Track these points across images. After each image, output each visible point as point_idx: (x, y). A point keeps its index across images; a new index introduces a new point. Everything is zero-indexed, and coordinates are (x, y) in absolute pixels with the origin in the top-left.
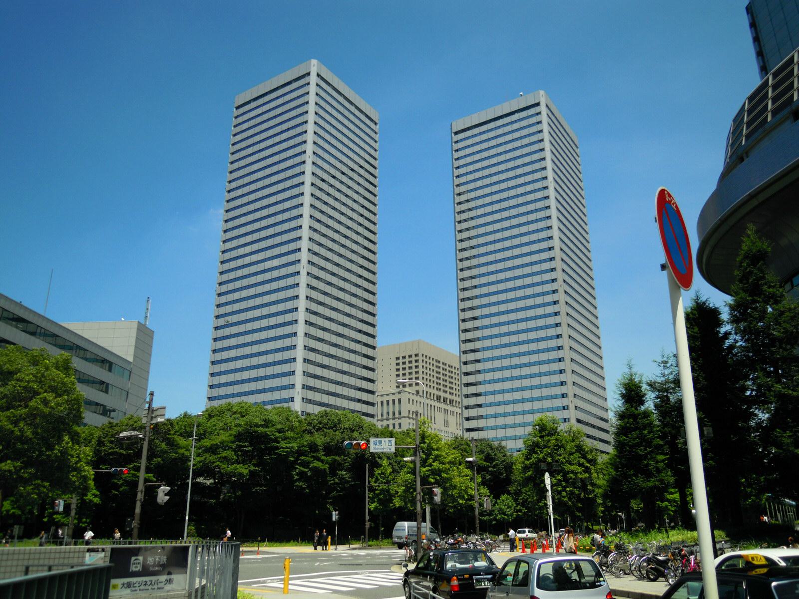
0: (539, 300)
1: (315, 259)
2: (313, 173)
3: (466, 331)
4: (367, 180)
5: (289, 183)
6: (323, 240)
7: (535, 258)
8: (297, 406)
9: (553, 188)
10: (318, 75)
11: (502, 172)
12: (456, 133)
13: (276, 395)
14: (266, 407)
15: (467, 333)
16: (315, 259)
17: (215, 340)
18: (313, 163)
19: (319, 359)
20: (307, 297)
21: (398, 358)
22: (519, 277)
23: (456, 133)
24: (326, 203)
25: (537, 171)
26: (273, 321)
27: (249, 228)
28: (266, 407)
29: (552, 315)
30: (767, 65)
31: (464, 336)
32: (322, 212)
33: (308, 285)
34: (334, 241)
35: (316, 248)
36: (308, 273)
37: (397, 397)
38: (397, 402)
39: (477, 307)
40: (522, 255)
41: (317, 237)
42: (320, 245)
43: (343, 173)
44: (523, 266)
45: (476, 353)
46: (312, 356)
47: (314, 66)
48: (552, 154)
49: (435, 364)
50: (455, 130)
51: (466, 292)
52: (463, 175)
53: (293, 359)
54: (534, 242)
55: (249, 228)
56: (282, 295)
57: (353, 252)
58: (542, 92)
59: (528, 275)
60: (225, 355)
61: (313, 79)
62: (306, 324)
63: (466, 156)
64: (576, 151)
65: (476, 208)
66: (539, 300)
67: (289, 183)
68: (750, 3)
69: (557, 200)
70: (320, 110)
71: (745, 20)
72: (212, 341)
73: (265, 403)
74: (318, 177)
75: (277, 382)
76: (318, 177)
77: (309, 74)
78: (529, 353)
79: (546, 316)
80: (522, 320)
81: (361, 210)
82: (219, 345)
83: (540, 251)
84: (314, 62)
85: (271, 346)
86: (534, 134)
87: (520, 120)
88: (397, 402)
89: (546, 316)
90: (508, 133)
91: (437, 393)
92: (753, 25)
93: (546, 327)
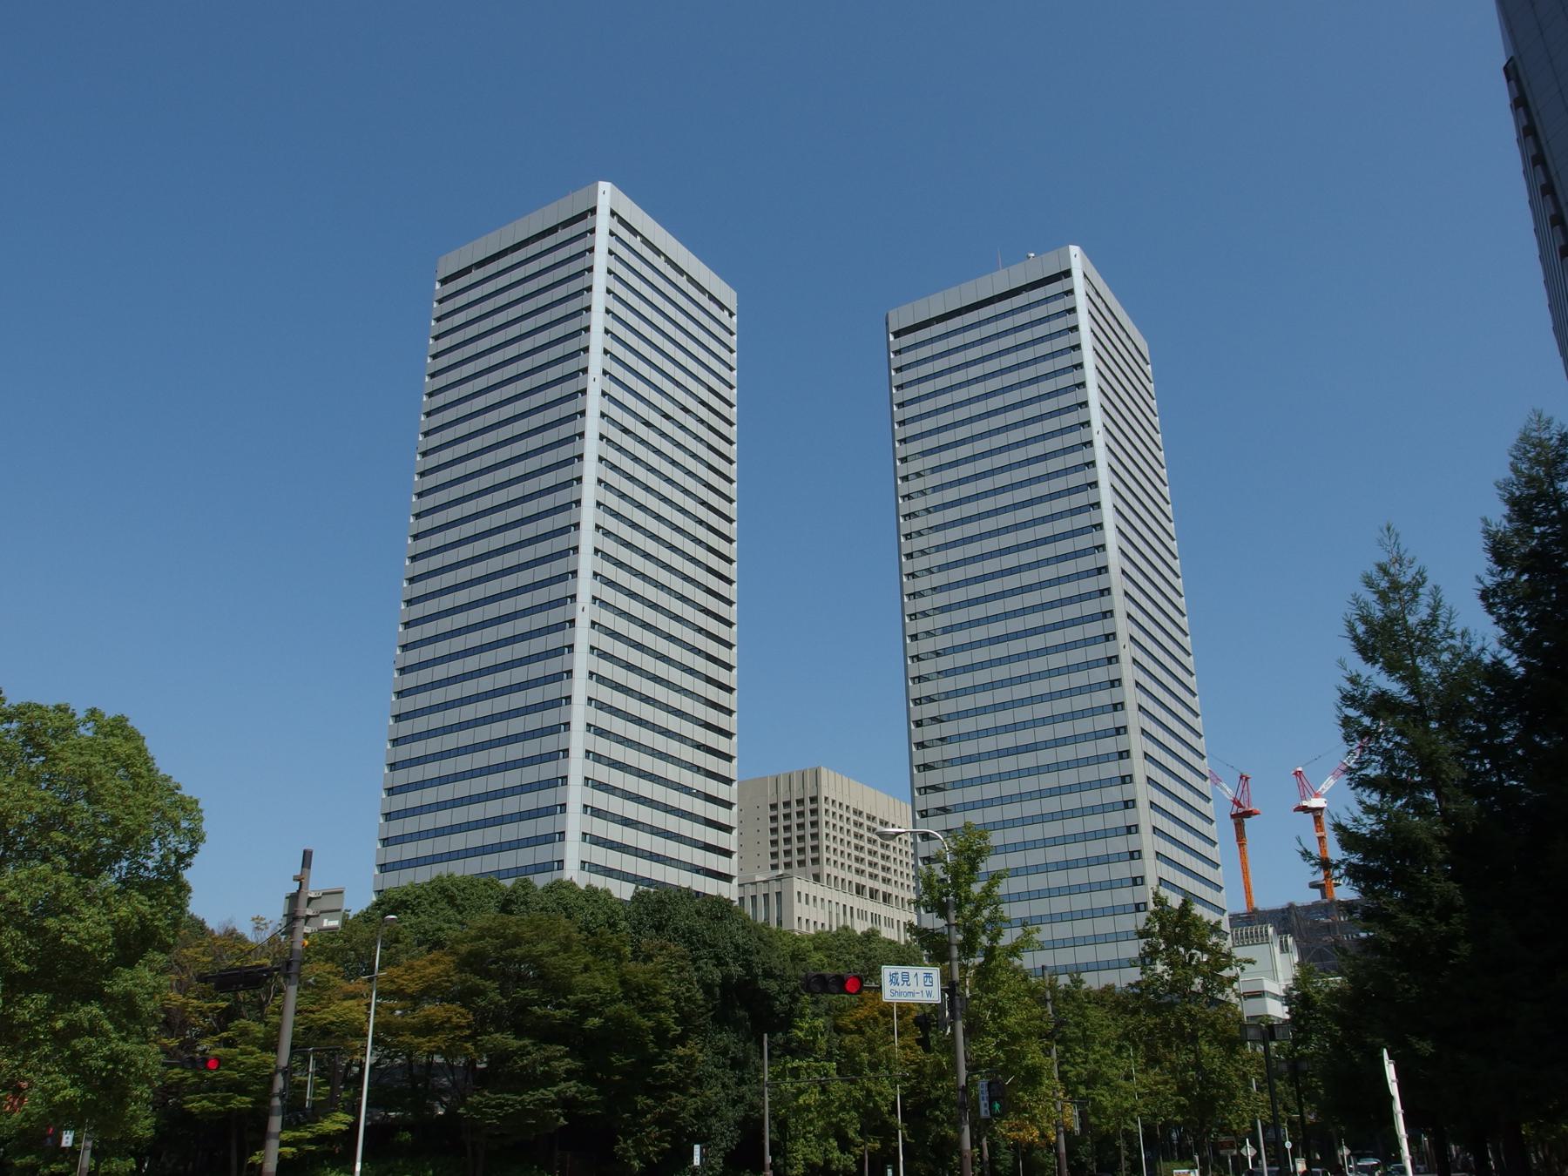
0: (1079, 679)
1: (609, 594)
2: (603, 415)
3: (926, 767)
4: (709, 680)
5: (557, 352)
6: (624, 555)
7: (1072, 611)
8: (572, 872)
9: (1109, 486)
10: (613, 213)
11: (996, 412)
12: (897, 334)
13: (526, 857)
14: (502, 882)
15: (928, 773)
16: (609, 594)
17: (391, 791)
18: (604, 394)
19: (616, 805)
20: (591, 674)
21: (774, 807)
22: (1044, 721)
23: (897, 334)
24: (631, 478)
25: (1064, 371)
26: (516, 726)
27: (468, 530)
28: (502, 882)
29: (1108, 733)
30: (1555, 180)
31: (923, 779)
32: (623, 496)
33: (592, 648)
34: (646, 556)
35: (607, 644)
36: (593, 623)
37: (775, 887)
38: (773, 899)
39: (950, 717)
40: (1052, 696)
41: (610, 547)
42: (616, 515)
43: (667, 416)
44: (1049, 673)
45: (942, 724)
46: (601, 800)
47: (606, 195)
48: (1102, 395)
49: (853, 817)
50: (894, 327)
51: (920, 601)
52: (913, 419)
53: (562, 778)
54: (1052, 414)
55: (468, 530)
56: (539, 620)
57: (686, 578)
58: (1074, 250)
59: (1061, 694)
60: (413, 799)
61: (603, 222)
62: (584, 840)
63: (921, 417)
64: (1148, 387)
65: (960, 737)
66: (1079, 679)
67: (557, 352)
68: (1511, 60)
69: (1123, 553)
70: (619, 245)
71: (1501, 95)
72: (386, 771)
73: (500, 874)
74: (613, 422)
75: (539, 620)
76: (613, 422)
77: (593, 211)
78: (1064, 840)
79: (1089, 665)
80: (1048, 768)
81: (702, 513)
82: (400, 802)
83: (1081, 598)
84: (605, 187)
85: (512, 778)
86: (1064, 371)
87: (1029, 306)
88: (773, 899)
89: (1089, 665)
90: (1006, 333)
91: (857, 879)
92: (1520, 103)
93: (1090, 688)
